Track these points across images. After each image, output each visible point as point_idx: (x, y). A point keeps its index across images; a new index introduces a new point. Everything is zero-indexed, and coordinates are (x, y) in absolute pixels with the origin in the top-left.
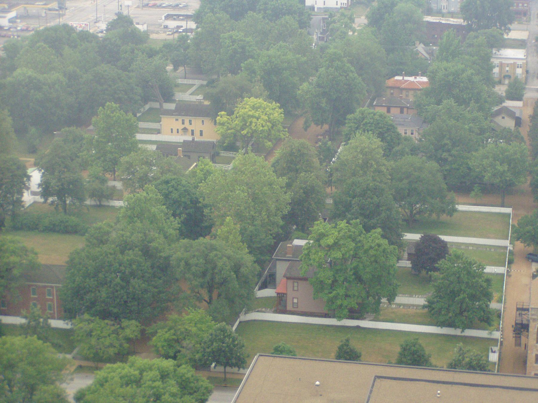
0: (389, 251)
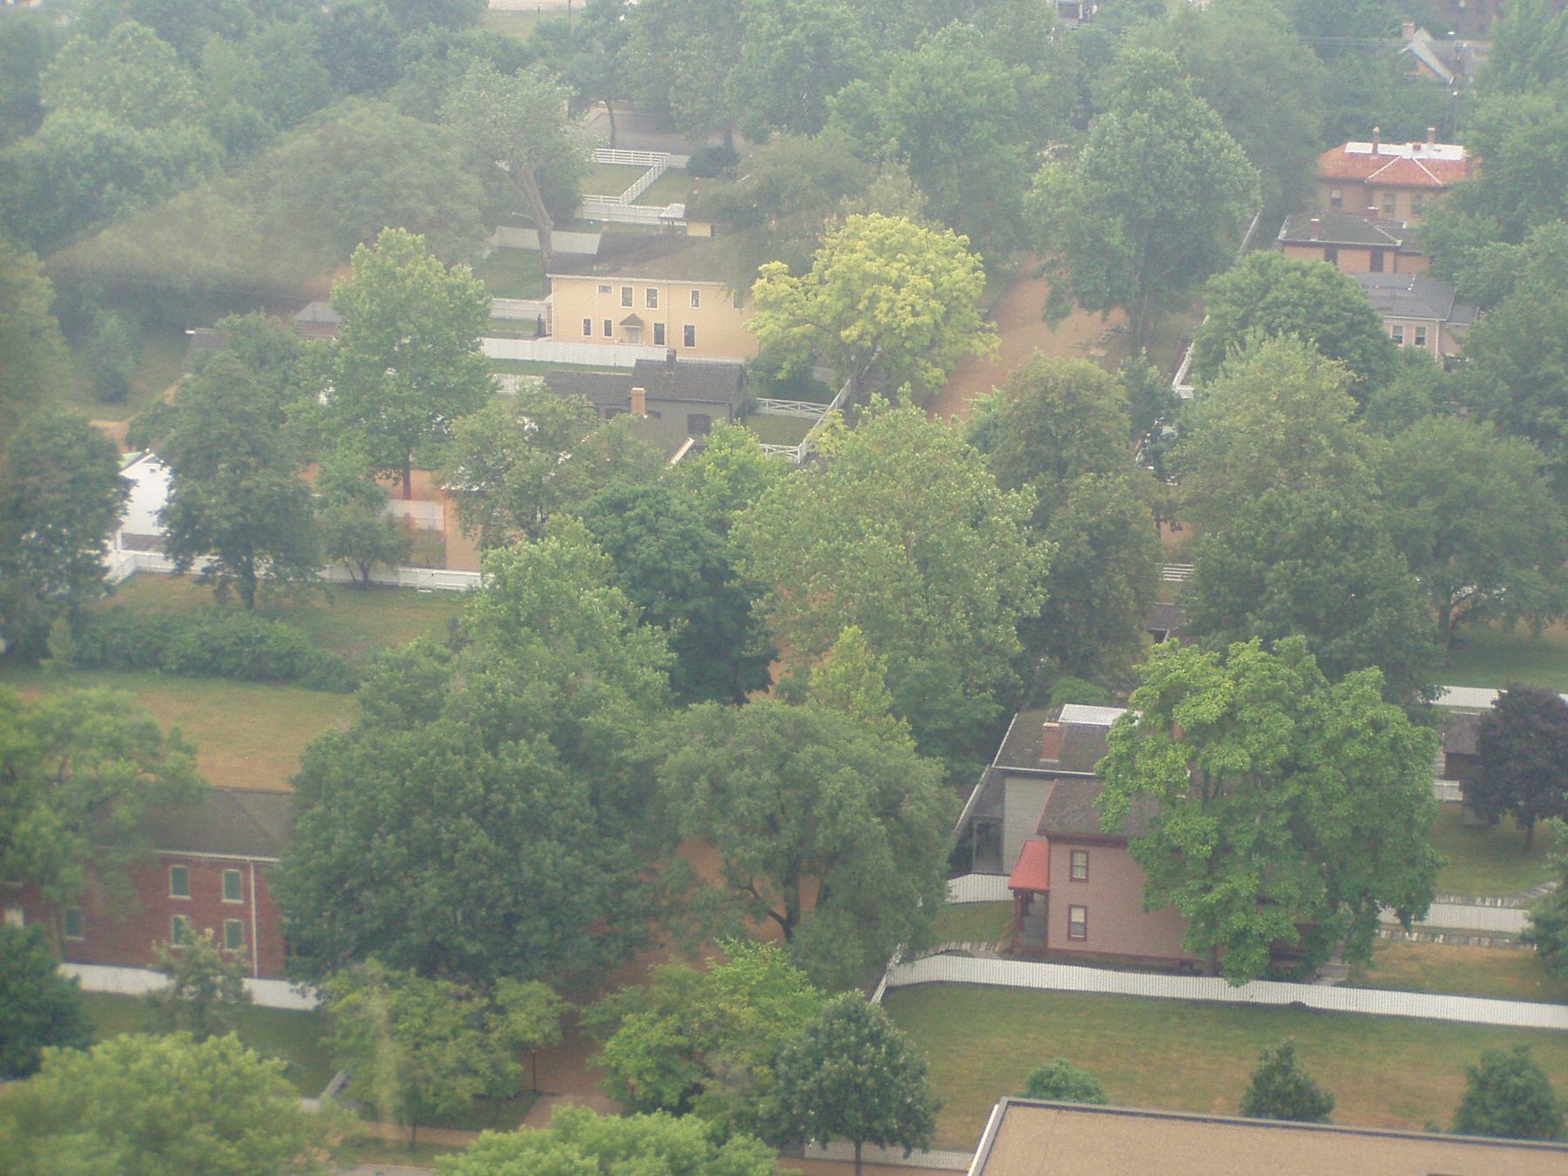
0: (1408, 744)
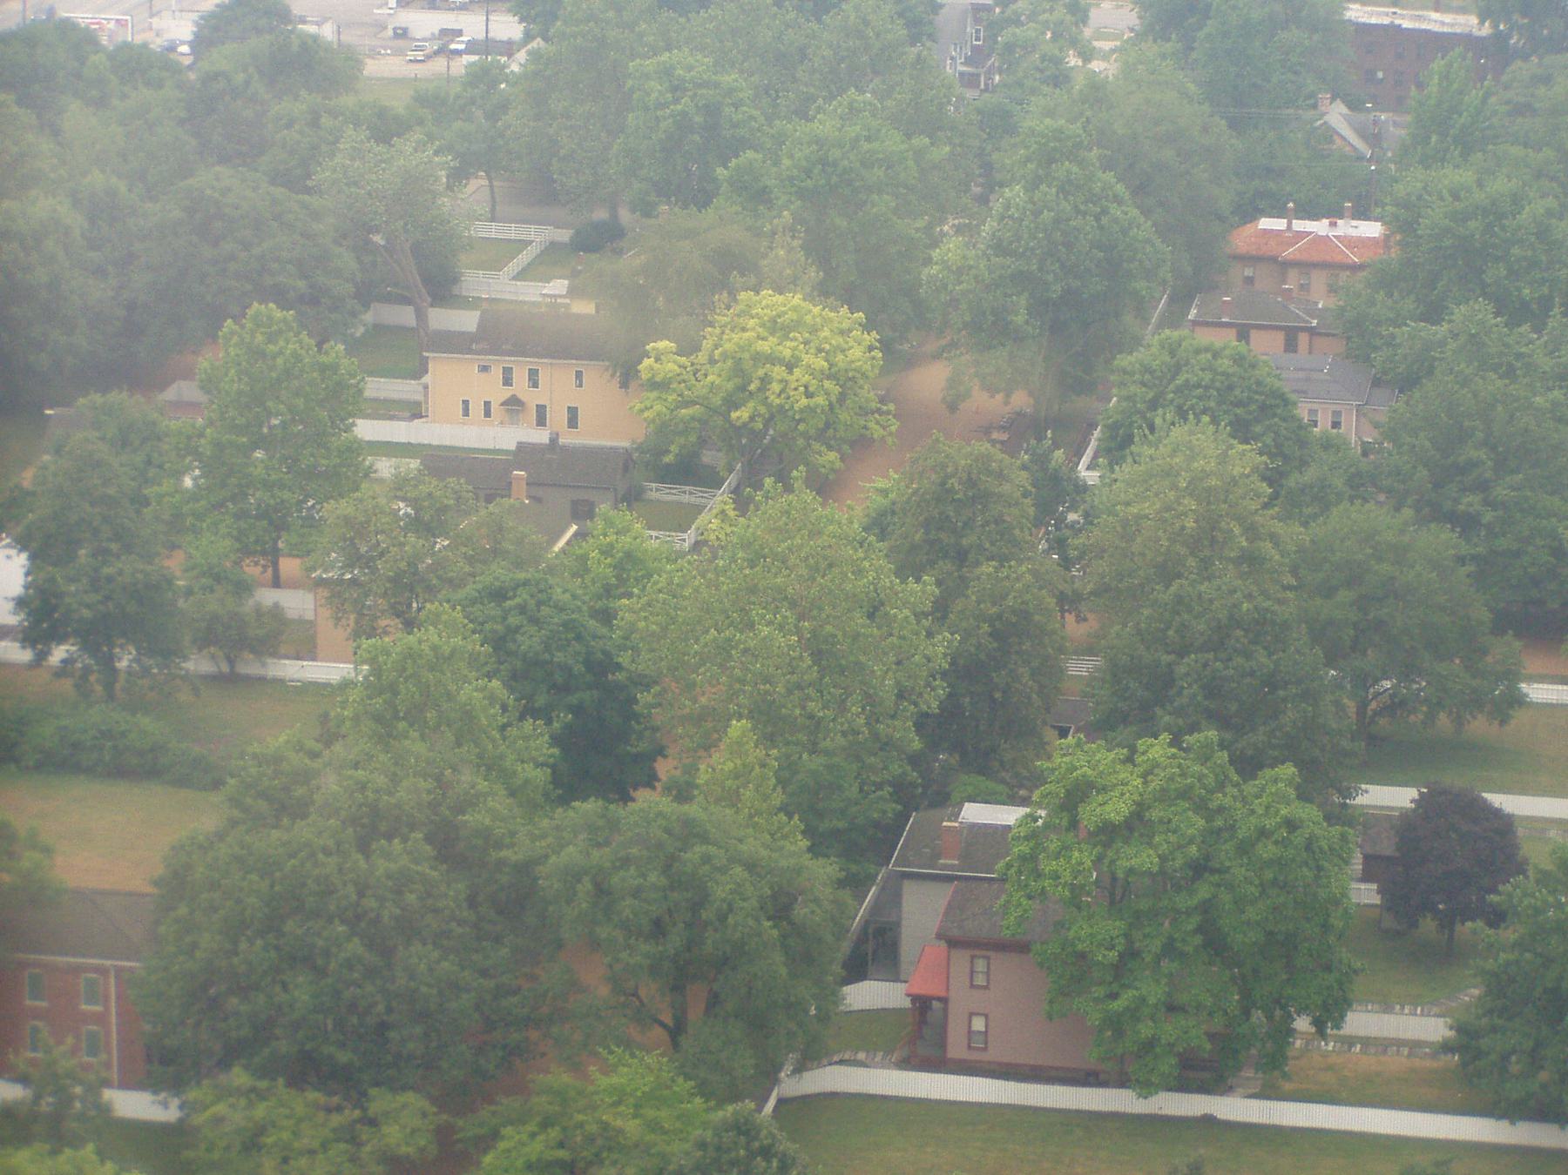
0: (1324, 844)
